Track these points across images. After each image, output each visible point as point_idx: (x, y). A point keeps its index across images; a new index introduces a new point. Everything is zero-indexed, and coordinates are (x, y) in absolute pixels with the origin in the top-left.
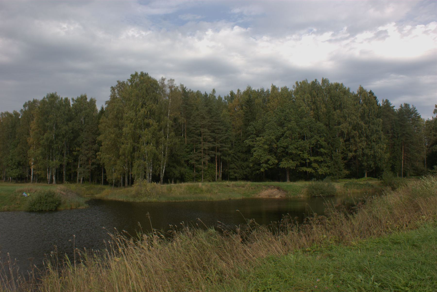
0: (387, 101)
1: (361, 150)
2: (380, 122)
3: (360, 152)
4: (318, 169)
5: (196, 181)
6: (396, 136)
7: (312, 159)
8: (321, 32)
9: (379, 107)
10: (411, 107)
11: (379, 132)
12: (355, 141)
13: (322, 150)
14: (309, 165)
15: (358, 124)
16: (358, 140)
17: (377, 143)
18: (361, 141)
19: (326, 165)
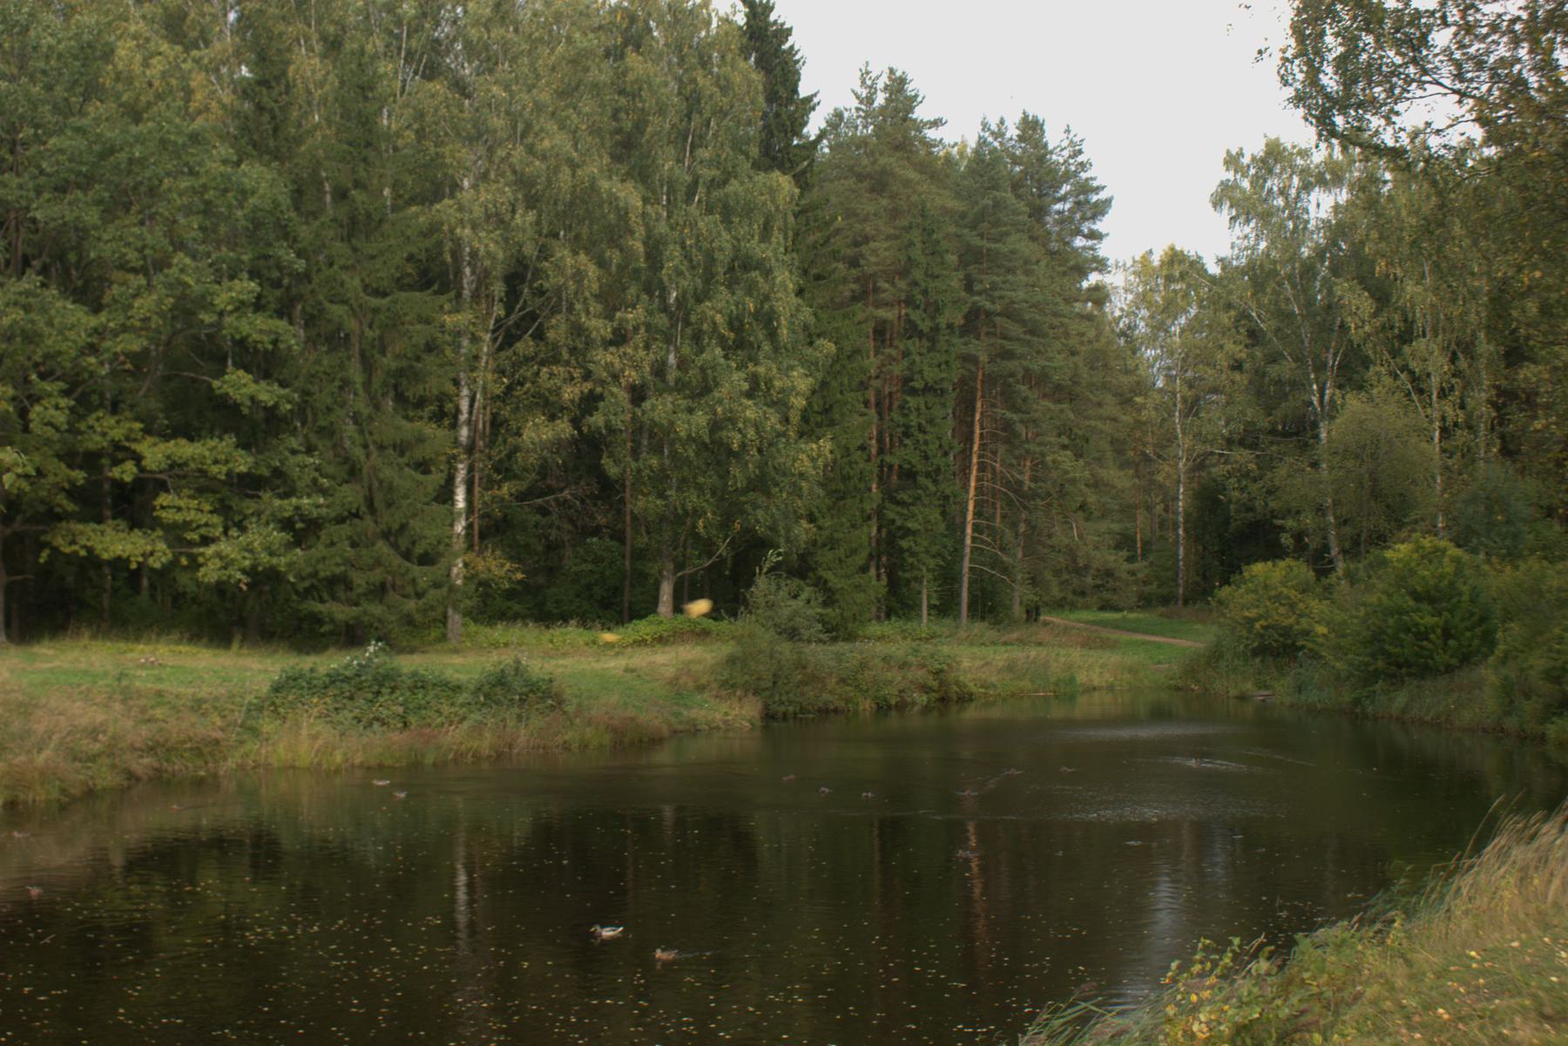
0: (898, 85)
1: (623, 396)
2: (772, 191)
3: (615, 411)
4: (206, 541)
5: (411, 876)
6: (925, 326)
7: (155, 453)
8: (1297, 30)
9: (1213, 280)
10: (1053, 137)
11: (768, 273)
12: (578, 330)
13: (238, 384)
14: (131, 504)
15: (586, 195)
16: (600, 327)
17: (739, 344)
18: (619, 338)
19: (286, 506)
